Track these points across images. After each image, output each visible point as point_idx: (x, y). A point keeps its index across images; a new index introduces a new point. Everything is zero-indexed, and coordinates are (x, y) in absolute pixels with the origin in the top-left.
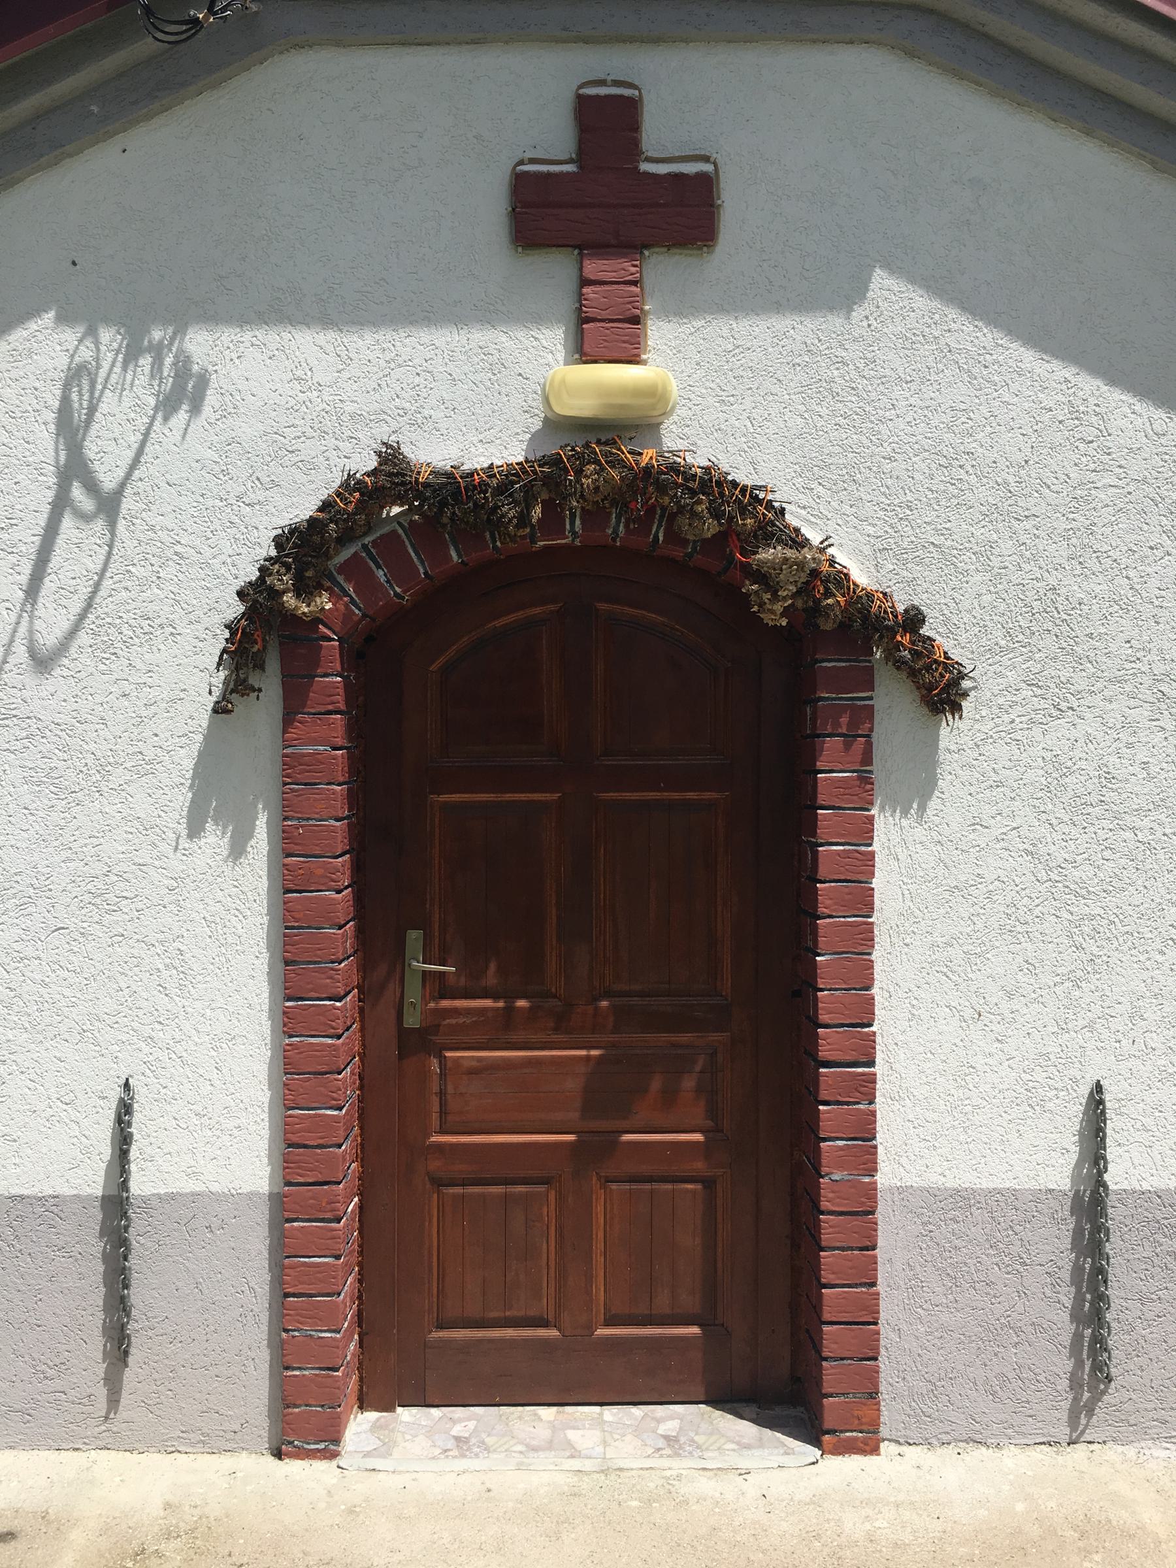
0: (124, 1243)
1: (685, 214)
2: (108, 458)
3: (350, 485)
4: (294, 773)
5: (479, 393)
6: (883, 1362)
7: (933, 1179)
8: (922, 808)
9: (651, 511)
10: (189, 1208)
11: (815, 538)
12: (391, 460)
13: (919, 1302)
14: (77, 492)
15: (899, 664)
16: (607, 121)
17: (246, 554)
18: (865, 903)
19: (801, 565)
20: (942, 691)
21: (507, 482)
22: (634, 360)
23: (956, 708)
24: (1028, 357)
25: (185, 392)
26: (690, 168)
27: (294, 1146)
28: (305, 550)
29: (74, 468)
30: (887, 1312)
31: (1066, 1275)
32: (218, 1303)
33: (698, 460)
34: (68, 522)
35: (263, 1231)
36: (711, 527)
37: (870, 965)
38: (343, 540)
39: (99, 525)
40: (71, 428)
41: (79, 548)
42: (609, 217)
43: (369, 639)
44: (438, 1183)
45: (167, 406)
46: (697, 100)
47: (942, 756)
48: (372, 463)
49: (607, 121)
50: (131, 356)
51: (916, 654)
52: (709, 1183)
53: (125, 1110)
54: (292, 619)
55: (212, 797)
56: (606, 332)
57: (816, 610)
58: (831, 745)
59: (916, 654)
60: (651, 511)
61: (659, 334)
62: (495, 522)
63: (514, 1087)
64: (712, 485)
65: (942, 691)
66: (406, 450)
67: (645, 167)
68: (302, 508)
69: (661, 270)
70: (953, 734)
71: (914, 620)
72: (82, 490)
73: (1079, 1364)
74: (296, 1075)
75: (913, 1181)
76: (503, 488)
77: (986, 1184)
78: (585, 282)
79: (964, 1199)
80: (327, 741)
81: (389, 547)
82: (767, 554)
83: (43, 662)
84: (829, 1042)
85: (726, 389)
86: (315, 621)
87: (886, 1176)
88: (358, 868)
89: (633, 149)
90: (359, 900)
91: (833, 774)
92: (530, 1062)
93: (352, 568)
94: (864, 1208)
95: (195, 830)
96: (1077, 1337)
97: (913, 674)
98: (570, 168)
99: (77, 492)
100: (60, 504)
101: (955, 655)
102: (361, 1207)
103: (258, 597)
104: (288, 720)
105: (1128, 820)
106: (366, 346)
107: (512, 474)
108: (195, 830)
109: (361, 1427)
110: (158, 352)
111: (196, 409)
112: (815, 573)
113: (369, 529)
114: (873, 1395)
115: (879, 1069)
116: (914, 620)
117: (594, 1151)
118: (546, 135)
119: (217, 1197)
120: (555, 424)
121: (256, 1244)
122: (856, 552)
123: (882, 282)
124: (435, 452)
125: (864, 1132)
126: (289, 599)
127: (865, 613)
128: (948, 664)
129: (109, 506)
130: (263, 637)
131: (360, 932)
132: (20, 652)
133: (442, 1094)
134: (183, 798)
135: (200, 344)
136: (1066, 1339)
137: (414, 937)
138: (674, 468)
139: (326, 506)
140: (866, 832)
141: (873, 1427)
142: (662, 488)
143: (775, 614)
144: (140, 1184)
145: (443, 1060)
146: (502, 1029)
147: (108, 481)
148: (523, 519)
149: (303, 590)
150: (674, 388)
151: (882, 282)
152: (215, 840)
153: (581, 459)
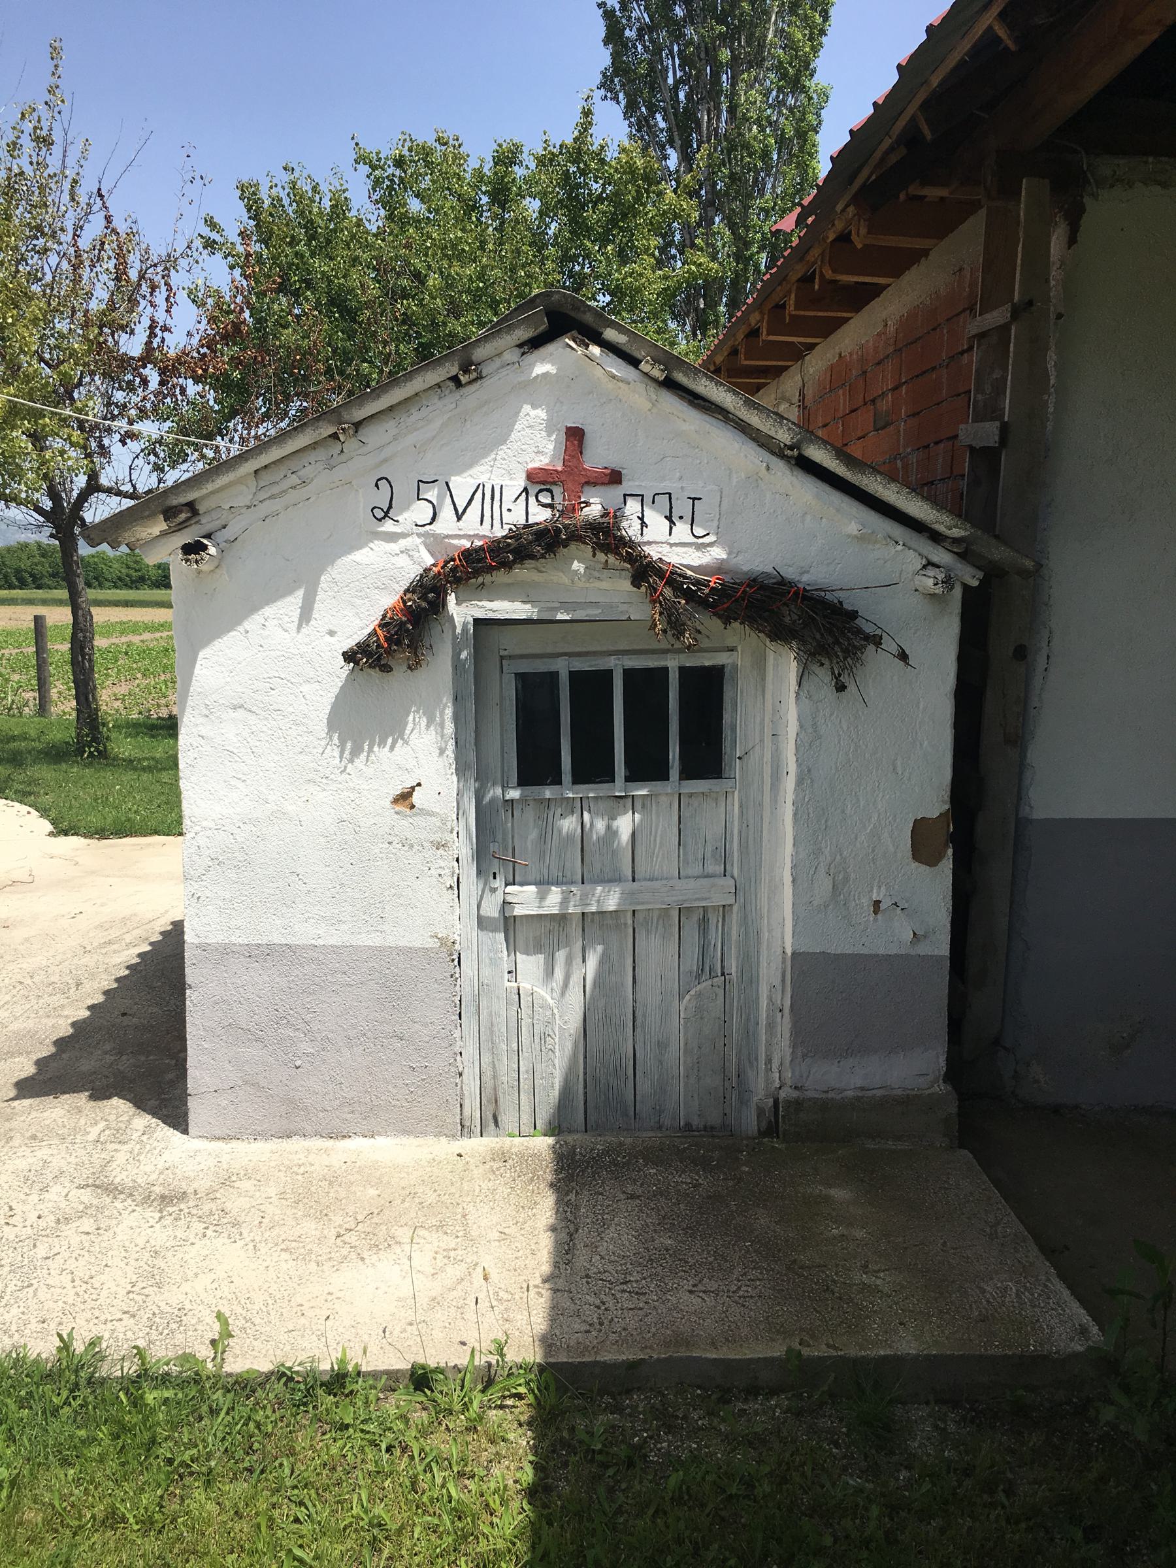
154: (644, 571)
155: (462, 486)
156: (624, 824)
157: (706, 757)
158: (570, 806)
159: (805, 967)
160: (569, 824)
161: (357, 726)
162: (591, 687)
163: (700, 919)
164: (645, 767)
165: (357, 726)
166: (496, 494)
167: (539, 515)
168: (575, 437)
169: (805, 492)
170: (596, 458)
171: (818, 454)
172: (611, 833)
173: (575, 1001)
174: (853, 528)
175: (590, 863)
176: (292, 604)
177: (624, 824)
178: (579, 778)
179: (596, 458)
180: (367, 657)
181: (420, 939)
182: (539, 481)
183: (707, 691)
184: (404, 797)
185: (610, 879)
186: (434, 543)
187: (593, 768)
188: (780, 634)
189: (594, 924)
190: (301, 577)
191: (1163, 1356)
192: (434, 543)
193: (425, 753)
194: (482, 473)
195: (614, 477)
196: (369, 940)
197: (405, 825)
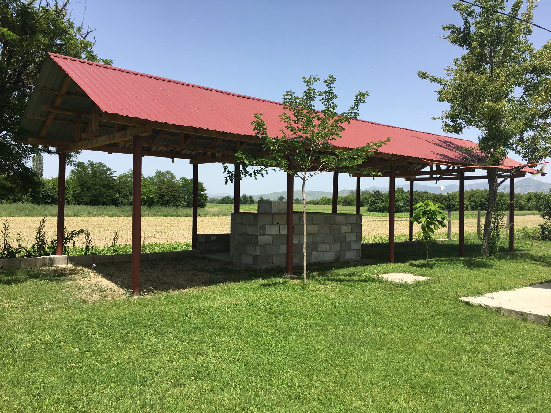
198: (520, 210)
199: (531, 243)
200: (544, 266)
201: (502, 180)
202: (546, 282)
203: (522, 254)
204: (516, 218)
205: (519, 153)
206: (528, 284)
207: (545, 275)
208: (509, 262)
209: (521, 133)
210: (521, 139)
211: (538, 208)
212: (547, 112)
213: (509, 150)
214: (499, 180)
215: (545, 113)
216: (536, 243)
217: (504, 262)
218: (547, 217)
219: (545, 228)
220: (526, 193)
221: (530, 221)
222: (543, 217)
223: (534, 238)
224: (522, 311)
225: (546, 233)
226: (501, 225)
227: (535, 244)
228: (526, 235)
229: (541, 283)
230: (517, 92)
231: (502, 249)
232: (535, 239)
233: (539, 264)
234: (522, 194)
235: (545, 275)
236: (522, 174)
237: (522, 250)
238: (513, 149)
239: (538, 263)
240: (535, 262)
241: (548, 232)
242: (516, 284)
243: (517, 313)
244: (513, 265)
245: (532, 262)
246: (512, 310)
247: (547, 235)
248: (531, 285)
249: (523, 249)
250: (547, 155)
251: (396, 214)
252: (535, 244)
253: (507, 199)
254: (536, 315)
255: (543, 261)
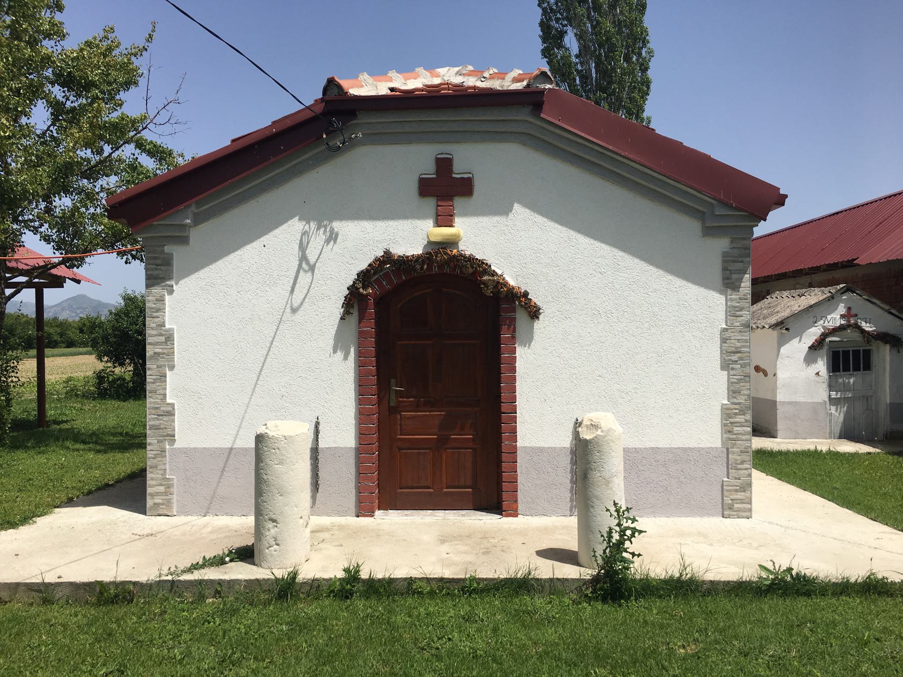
0: (317, 459)
1: (465, 187)
2: (312, 256)
3: (377, 259)
4: (361, 334)
5: (410, 236)
6: (519, 493)
7: (533, 444)
8: (530, 345)
9: (455, 266)
10: (334, 451)
11: (499, 272)
12: (387, 253)
13: (527, 479)
14: (304, 266)
15: (522, 306)
16: (444, 165)
17: (350, 278)
18: (514, 370)
19: (494, 281)
20: (534, 313)
21: (417, 259)
22: (451, 226)
23: (538, 318)
24: (557, 226)
25: (333, 237)
26: (465, 176)
27: (362, 434)
28: (364, 277)
29: (303, 258)
30: (520, 479)
31: (569, 470)
32: (343, 477)
33: (468, 253)
34: (302, 273)
35: (353, 457)
36: (471, 270)
37: (515, 387)
38: (375, 274)
39: (310, 274)
40: (303, 248)
41: (305, 278)
42: (445, 190)
43: (380, 299)
44: (400, 449)
45: (327, 241)
46: (468, 158)
47: (535, 330)
48: (382, 254)
49: (444, 165)
50: (318, 229)
51: (526, 304)
52: (474, 450)
53: (317, 425)
54: (362, 294)
55: (339, 344)
56: (444, 219)
57: (499, 292)
58: (505, 328)
59: (526, 304)
60: (455, 266)
61: (458, 221)
62: (414, 269)
63: (421, 423)
64: (471, 259)
65: (534, 313)
66: (393, 251)
67: (454, 176)
68: (364, 266)
69: (459, 203)
70: (538, 325)
71: (526, 294)
72: (306, 264)
73: (572, 495)
74: (362, 416)
75: (528, 445)
76: (416, 261)
77: (547, 446)
78: (438, 206)
79: (541, 450)
80: (370, 327)
81: (386, 275)
82: (486, 278)
83: (294, 311)
84: (504, 407)
85: (476, 235)
86: (367, 295)
87: (519, 444)
88: (377, 361)
89: (451, 171)
90: (378, 370)
91: (505, 336)
92: (424, 416)
93: (377, 281)
94: (514, 451)
95: (335, 352)
96: (572, 487)
97: (526, 308)
98: (434, 176)
99: (304, 266)
100: (300, 266)
101: (538, 303)
102: (379, 455)
103: (353, 289)
104: (360, 322)
105: (585, 348)
106: (381, 225)
107: (419, 257)
108: (335, 352)
109: (378, 513)
110: (325, 227)
111: (335, 242)
112: (498, 282)
113: (381, 271)
114: (516, 501)
115: (518, 415)
116: (526, 294)
117: (442, 442)
118: (429, 169)
119: (341, 448)
120: (430, 243)
121: (352, 461)
122: (511, 276)
123: (516, 206)
124: (399, 251)
125: (514, 431)
126: (361, 290)
127: (512, 293)
128: (536, 306)
129: (312, 268)
130: (354, 300)
131: (378, 379)
132: (288, 310)
133: (401, 425)
134: (332, 342)
135: (336, 225)
136: (569, 488)
137: (393, 381)
138: (461, 255)
139: (370, 265)
140: (514, 351)
141: (516, 510)
142: (458, 261)
143: (489, 293)
144: (322, 445)
145: (401, 415)
146: (417, 407)
147: (312, 260)
148: (422, 268)
149: (364, 287)
150: (462, 234)
151: (516, 206)
152: (340, 355)
153: (437, 253)
154: (863, 331)
155: (829, 317)
156: (852, 381)
157: (868, 367)
158: (841, 377)
159: (893, 406)
160: (840, 380)
161: (810, 359)
162: (846, 353)
163: (867, 398)
164: (857, 368)
165: (810, 359)
166: (835, 319)
167: (843, 322)
168: (849, 309)
169: (891, 317)
170: (853, 312)
171: (893, 311)
172: (849, 382)
173: (842, 415)
174: (396, 572)
175: (845, 388)
176: (798, 339)
177: (852, 381)
178: (844, 371)
179: (853, 312)
180: (812, 348)
181: (820, 401)
182: (842, 316)
183: (867, 354)
184: (817, 374)
185: (849, 391)
186: (824, 327)
187: (846, 369)
188: (886, 343)
189: (846, 400)
190: (800, 334)
191: (220, 478)
192: (824, 327)
193: (821, 366)
194: (832, 315)
195: (856, 315)
196: (810, 401)
197: (817, 378)
198: (68, 347)
199: (80, 405)
200: (99, 452)
201: (12, 290)
202: (99, 489)
203: (61, 430)
204: (48, 362)
205: (47, 239)
206: (65, 499)
207: (97, 473)
208: (32, 452)
209: (47, 198)
210: (48, 210)
211: (94, 344)
212: (96, 166)
213: (26, 231)
214: (8, 292)
215: (93, 167)
216: (89, 405)
217: (20, 454)
218: (106, 359)
219: (104, 377)
220: (77, 319)
221: (83, 364)
222: (100, 358)
223: (86, 396)
224: (38, 580)
225: (106, 385)
226: (15, 379)
227: (86, 408)
228: (73, 392)
229: (90, 492)
230: (39, 117)
231: (19, 425)
232: (87, 398)
233: (90, 450)
234: (70, 320)
235: (97, 473)
236: (58, 282)
237: (63, 422)
238: (35, 230)
239: (87, 447)
240: (82, 446)
241: (109, 382)
242: (37, 507)
243: (31, 588)
244: (42, 459)
245: (78, 446)
246: (18, 584)
247: (106, 389)
248: (70, 502)
249: (65, 418)
250: (98, 245)
251: (47, 351)
252: (86, 408)
253: (32, 332)
254: (71, 584)
255: (96, 443)
